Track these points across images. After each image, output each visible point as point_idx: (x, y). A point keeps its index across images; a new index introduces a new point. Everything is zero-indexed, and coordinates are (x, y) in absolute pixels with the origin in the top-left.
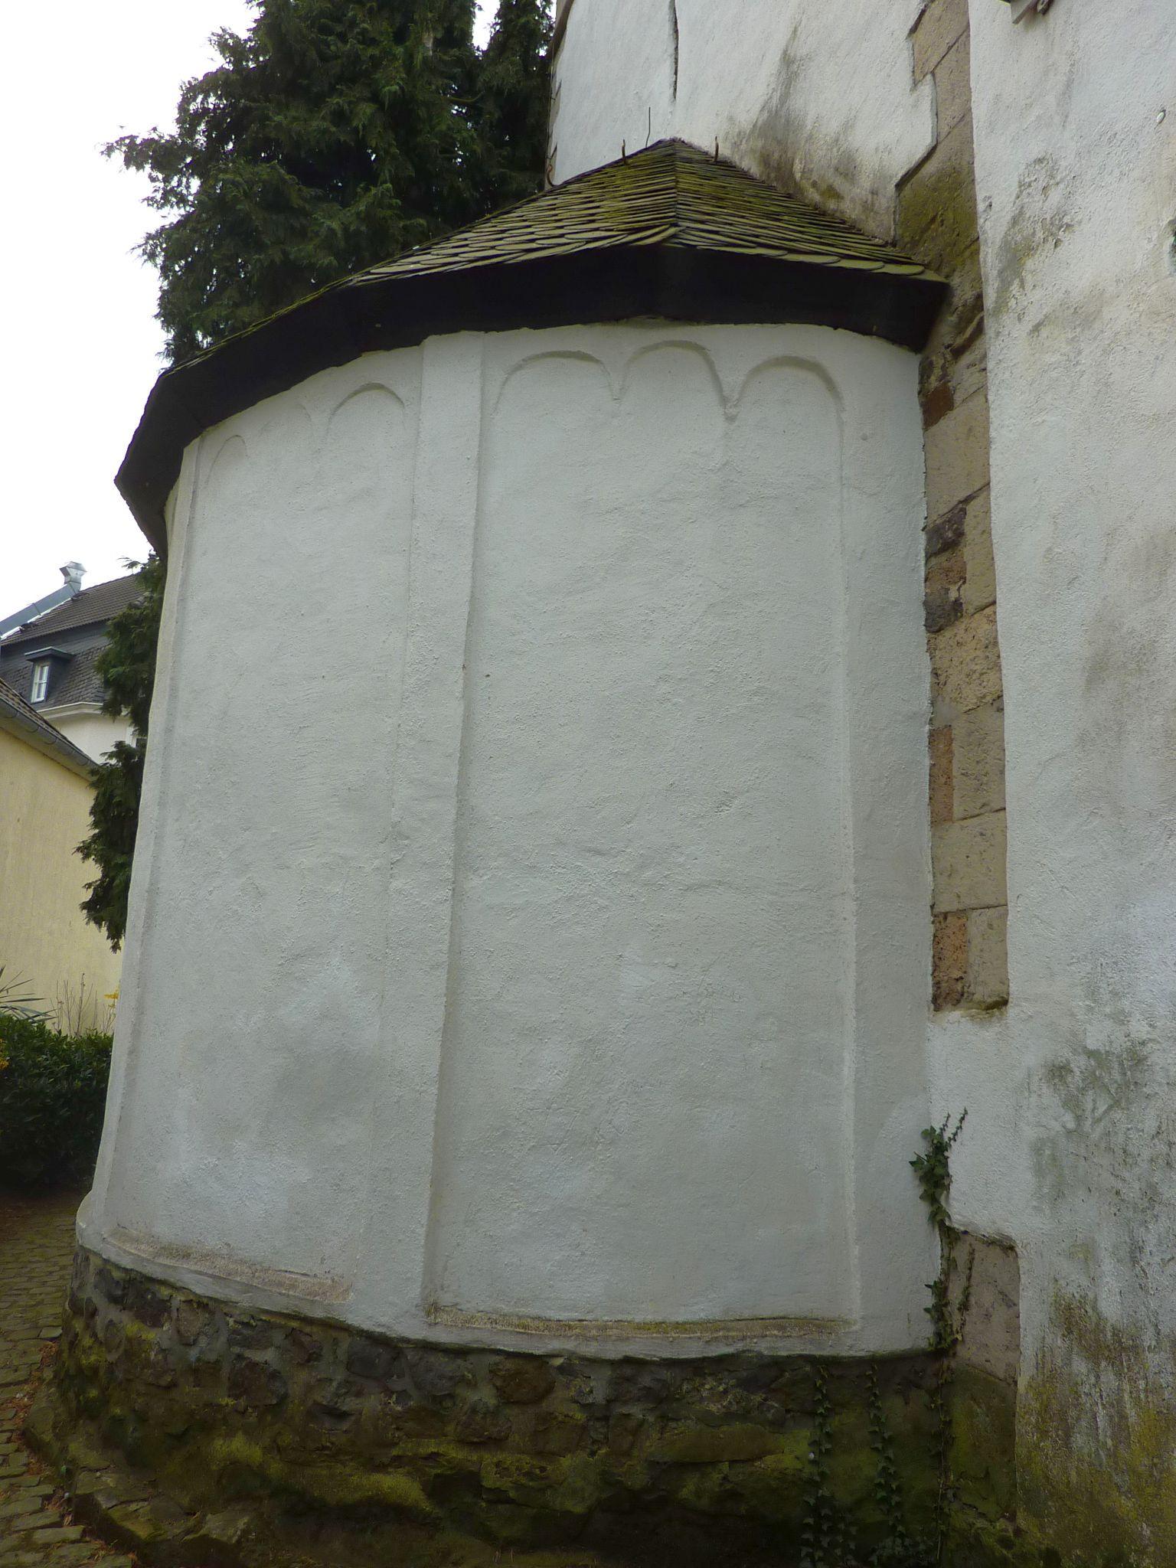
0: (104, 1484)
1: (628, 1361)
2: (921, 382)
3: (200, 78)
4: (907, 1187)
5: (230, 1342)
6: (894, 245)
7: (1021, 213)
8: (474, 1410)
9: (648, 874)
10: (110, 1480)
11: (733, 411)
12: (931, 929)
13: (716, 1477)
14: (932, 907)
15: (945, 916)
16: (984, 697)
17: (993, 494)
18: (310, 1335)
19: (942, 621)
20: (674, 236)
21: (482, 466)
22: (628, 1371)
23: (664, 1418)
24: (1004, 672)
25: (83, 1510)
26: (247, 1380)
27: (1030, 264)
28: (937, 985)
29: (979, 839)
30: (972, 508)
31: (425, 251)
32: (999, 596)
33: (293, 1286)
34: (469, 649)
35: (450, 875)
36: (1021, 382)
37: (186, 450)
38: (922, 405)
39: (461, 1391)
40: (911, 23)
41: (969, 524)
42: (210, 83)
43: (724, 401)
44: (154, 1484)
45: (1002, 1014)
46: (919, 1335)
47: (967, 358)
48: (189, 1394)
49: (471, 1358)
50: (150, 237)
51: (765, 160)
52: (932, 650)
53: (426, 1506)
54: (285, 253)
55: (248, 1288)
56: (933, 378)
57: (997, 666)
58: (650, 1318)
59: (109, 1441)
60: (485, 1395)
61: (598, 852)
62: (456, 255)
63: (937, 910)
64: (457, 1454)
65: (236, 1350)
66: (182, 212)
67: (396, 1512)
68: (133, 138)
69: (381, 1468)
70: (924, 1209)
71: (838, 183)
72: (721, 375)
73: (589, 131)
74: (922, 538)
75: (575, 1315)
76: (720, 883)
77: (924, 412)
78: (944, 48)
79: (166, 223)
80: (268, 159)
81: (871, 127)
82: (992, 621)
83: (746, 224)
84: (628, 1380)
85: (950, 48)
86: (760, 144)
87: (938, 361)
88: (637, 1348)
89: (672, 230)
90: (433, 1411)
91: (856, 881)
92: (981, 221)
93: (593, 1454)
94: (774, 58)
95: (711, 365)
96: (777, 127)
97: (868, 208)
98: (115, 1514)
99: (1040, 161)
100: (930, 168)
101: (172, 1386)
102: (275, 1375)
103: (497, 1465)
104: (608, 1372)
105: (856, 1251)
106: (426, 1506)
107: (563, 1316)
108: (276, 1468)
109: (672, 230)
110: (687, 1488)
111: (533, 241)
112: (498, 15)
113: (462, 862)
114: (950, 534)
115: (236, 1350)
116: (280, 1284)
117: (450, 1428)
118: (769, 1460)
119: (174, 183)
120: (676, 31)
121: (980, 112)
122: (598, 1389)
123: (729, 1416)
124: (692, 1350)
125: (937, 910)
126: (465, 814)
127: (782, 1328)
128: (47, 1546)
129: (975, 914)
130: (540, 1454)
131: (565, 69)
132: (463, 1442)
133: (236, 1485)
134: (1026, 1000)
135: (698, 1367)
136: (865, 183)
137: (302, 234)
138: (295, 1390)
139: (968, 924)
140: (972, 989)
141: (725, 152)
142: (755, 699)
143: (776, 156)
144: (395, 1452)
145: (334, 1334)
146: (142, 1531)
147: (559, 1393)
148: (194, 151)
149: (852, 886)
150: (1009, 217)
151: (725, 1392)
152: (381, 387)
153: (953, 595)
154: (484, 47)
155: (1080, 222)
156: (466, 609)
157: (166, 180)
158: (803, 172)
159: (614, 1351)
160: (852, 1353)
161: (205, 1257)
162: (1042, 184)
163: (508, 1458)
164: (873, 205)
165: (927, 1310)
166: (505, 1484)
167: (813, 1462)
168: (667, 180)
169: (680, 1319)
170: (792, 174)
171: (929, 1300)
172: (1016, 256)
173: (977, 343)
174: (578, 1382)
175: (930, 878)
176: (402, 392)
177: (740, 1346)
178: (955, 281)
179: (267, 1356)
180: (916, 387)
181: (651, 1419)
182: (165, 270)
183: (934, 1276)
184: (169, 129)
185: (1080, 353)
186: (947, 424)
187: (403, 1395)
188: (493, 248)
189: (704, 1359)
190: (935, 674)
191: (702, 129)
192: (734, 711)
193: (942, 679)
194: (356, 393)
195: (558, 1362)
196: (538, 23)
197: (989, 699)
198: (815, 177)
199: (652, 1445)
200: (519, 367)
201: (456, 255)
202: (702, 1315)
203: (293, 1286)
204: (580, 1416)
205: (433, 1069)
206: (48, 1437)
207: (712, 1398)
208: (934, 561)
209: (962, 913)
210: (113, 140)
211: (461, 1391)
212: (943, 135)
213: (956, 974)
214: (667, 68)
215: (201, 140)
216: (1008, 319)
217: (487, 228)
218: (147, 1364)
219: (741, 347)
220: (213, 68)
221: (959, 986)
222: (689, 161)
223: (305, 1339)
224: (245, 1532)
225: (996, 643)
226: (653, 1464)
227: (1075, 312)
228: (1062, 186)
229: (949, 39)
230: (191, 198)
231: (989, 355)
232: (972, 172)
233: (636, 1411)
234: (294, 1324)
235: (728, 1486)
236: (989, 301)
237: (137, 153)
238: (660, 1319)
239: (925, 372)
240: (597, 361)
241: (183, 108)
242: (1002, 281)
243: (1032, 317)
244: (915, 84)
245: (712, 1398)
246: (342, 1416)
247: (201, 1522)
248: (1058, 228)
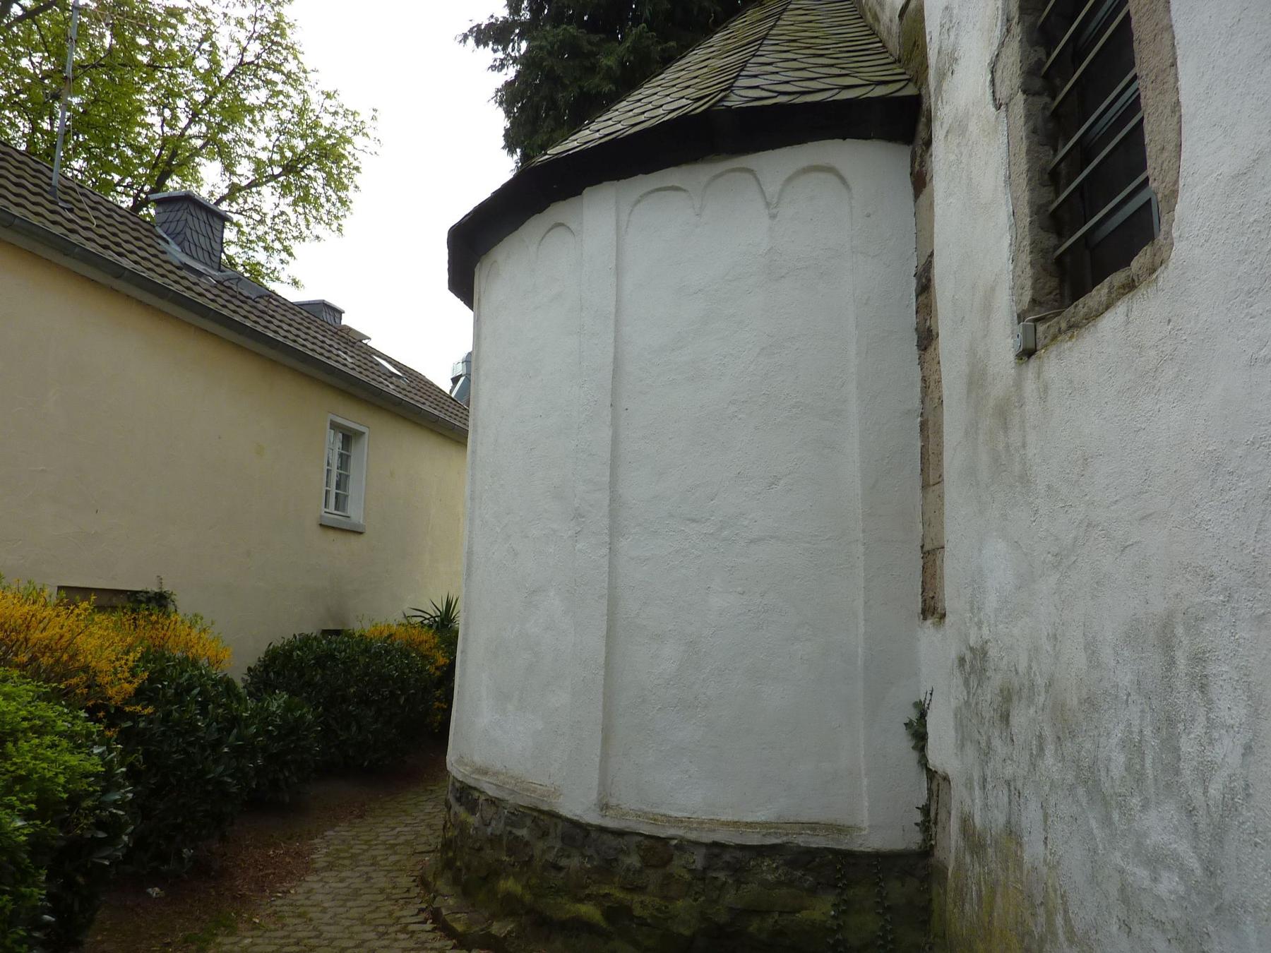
0: (448, 902)
1: (715, 844)
4: (904, 743)
5: (506, 824)
8: (628, 869)
10: (451, 902)
11: (774, 211)
13: (771, 921)
14: (922, 547)
18: (544, 820)
21: (619, 272)
22: (716, 851)
23: (739, 883)
25: (436, 916)
26: (515, 846)
28: (924, 601)
33: (534, 792)
34: (615, 393)
35: (607, 539)
37: (476, 270)
39: (621, 857)
43: (768, 205)
44: (473, 905)
46: (914, 840)
48: (488, 854)
49: (626, 838)
50: (498, 91)
53: (603, 924)
54: (581, 88)
55: (512, 792)
58: (730, 818)
59: (456, 881)
60: (634, 861)
61: (694, 521)
64: (619, 894)
65: (509, 828)
67: (581, 926)
68: (479, 26)
69: (581, 901)
70: (914, 755)
74: (914, 282)
75: (686, 815)
76: (772, 537)
84: (716, 856)
87: (919, 152)
88: (721, 836)
90: (607, 868)
91: (864, 531)
93: (696, 900)
98: (448, 918)
101: (480, 849)
102: (527, 844)
103: (642, 902)
104: (704, 850)
105: (865, 781)
106: (603, 924)
107: (679, 815)
108: (528, 898)
110: (754, 926)
113: (615, 532)
115: (509, 828)
116: (528, 790)
117: (616, 879)
118: (805, 914)
119: (510, 50)
122: (698, 860)
123: (779, 883)
124: (754, 839)
125: (926, 549)
126: (615, 500)
127: (814, 829)
128: (413, 932)
130: (665, 898)
132: (623, 888)
133: (510, 906)
135: (760, 851)
137: (592, 70)
138: (537, 852)
144: (587, 892)
145: (555, 820)
146: (459, 927)
147: (676, 862)
148: (522, 24)
151: (777, 868)
157: (504, 49)
159: (707, 838)
160: (862, 849)
161: (496, 774)
163: (647, 899)
165: (917, 824)
166: (646, 914)
167: (833, 917)
169: (749, 820)
171: (919, 817)
172: (942, 76)
174: (686, 856)
176: (573, 227)
177: (785, 839)
179: (523, 832)
181: (730, 881)
183: (922, 802)
184: (502, 13)
187: (591, 858)
189: (762, 846)
190: (924, 380)
195: (675, 842)
199: (730, 898)
200: (639, 201)
202: (763, 818)
203: (534, 792)
204: (687, 876)
205: (602, 660)
206: (430, 879)
207: (768, 871)
210: (466, 31)
211: (621, 857)
218: (470, 836)
219: (775, 165)
223: (541, 823)
224: (510, 932)
226: (731, 909)
233: (722, 876)
234: (535, 814)
238: (736, 819)
245: (768, 871)
246: (560, 869)
247: (491, 925)
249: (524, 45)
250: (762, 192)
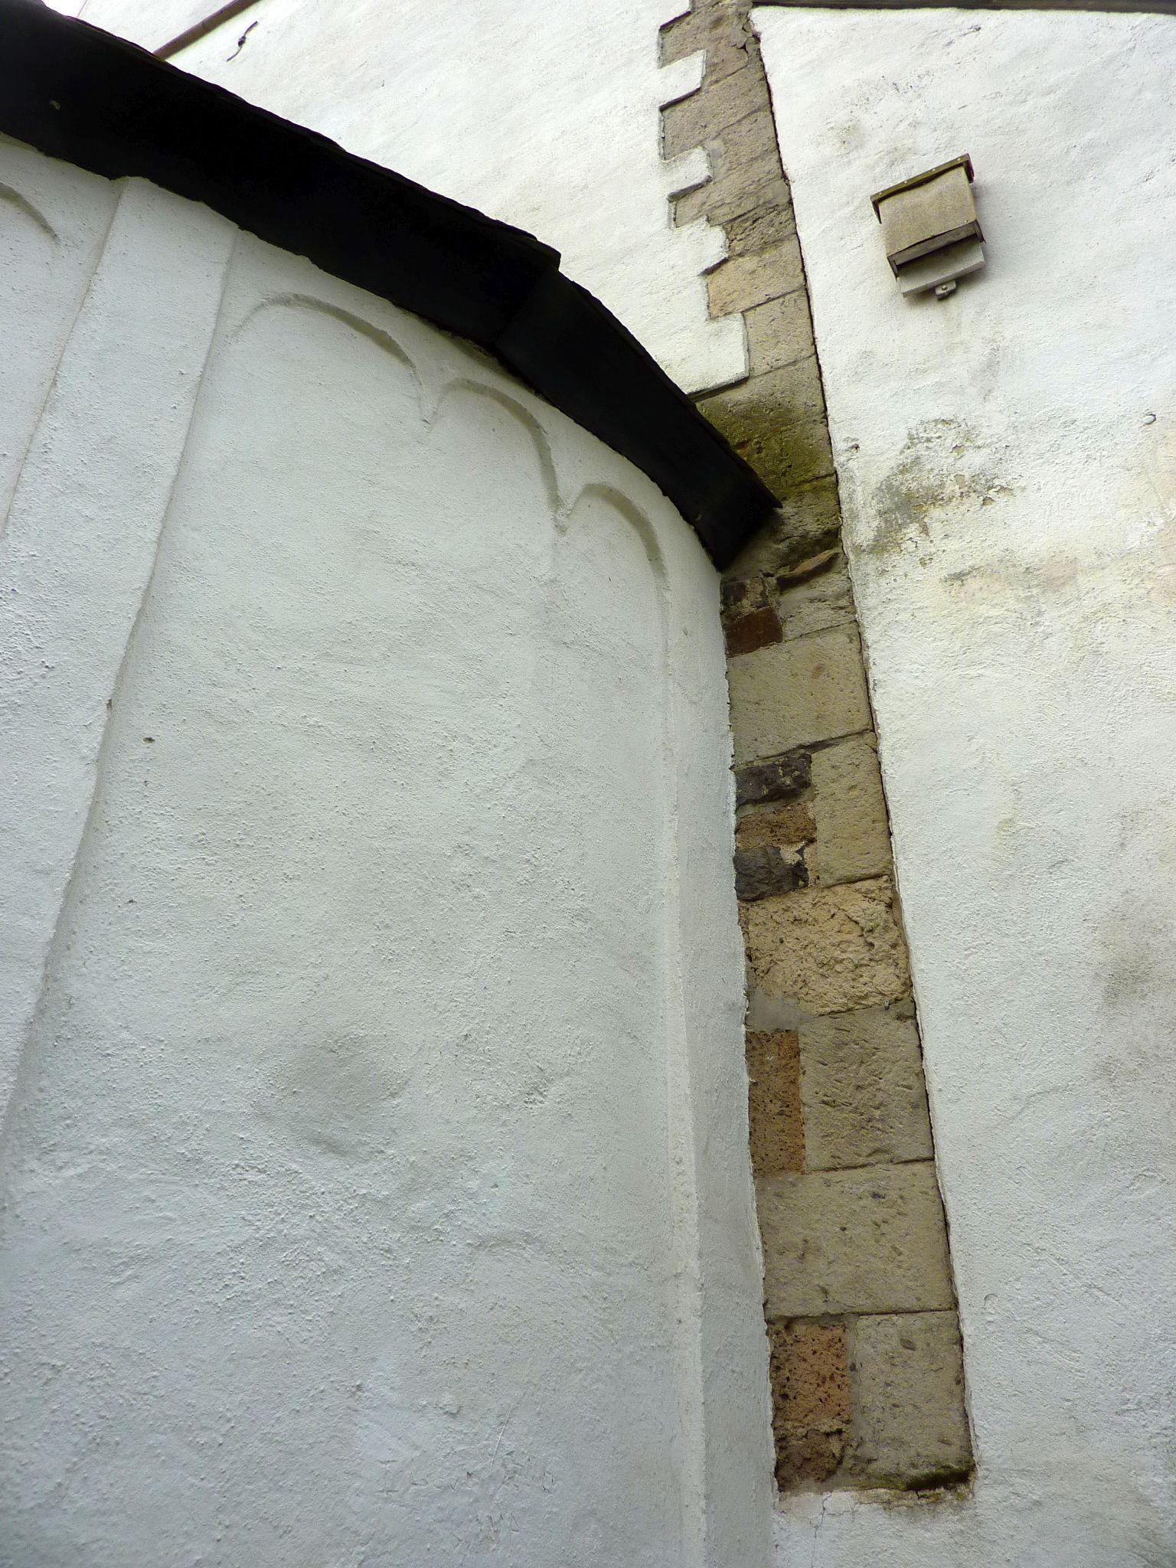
9: (419, 1206)
12: (765, 1347)
15: (790, 1322)
19: (764, 888)
28: (781, 1442)
29: (869, 1202)
38: (724, 627)
43: (556, 501)
45: (962, 1498)
52: (744, 923)
63: (774, 1313)
74: (731, 778)
76: (529, 1239)
77: (728, 636)
100: (740, 395)
129: (864, 1321)
134: (1022, 1472)
139: (849, 1338)
140: (868, 1450)
142: (578, 924)
149: (694, 1264)
153: (789, 855)
155: (1024, 489)
156: (134, 602)
173: (821, 580)
175: (759, 1258)
180: (719, 607)
192: (549, 934)
193: (763, 964)
208: (750, 810)
209: (837, 1320)
212: (761, 367)
213: (827, 1424)
221: (835, 1446)
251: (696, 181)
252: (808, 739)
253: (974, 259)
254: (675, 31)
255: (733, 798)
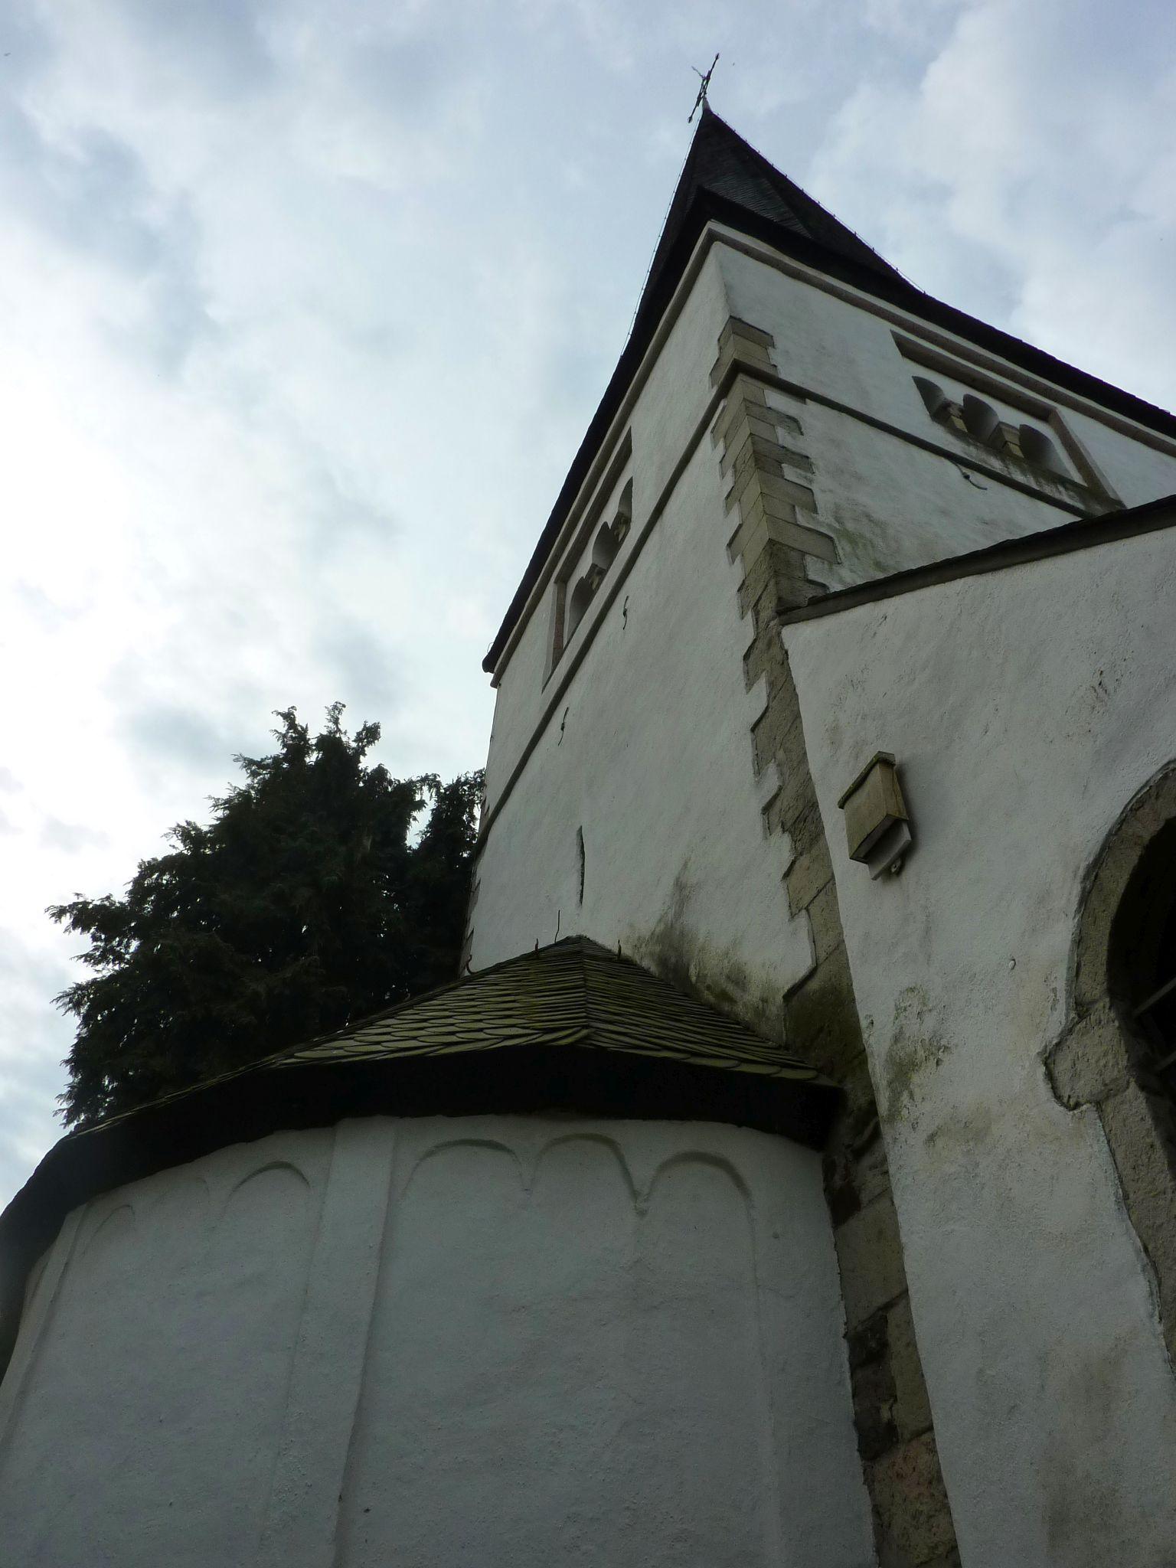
2: (825, 1179)
3: (160, 859)
6: (787, 1048)
7: (901, 1032)
16: (936, 1547)
17: (913, 1305)
20: (587, 1037)
24: (955, 1516)
27: (916, 1079)
30: (894, 1316)
31: (349, 1033)
32: (935, 1422)
36: (917, 1172)
40: (785, 869)
41: (892, 1332)
42: (168, 864)
43: (635, 1194)
47: (867, 1161)
51: (663, 962)
52: (870, 1481)
56: (837, 1177)
57: (945, 1508)
62: (378, 1043)
66: (117, 968)
68: (85, 904)
71: (730, 988)
72: (631, 1170)
73: (503, 927)
78: (814, 892)
79: (99, 976)
80: (208, 928)
81: (759, 948)
82: (933, 1451)
83: (650, 1025)
85: (819, 892)
86: (658, 949)
89: (585, 1032)
92: (865, 1036)
94: (668, 883)
95: (621, 1160)
96: (673, 944)
97: (760, 1013)
99: (912, 990)
100: (814, 985)
109: (585, 1032)
111: (453, 1033)
112: (429, 826)
114: (873, 1345)
119: (115, 943)
120: (583, 853)
121: (852, 945)
131: (484, 869)
136: (753, 995)
141: (627, 951)
143: (673, 960)
148: (139, 917)
150: (890, 1035)
152: (287, 1166)
153: (885, 1415)
154: (415, 847)
157: (108, 940)
158: (698, 976)
162: (916, 1009)
164: (764, 1010)
168: (576, 977)
170: (688, 977)
172: (903, 1071)
178: (848, 1086)
180: (822, 1185)
182: (87, 1020)
185: (977, 1164)
186: (857, 1225)
188: (414, 1038)
190: (877, 1511)
191: (608, 931)
194: (261, 1171)
196: (463, 833)
197: (941, 1550)
198: (709, 981)
201: (378, 1043)
212: (823, 955)
214: (575, 879)
215: (148, 908)
216: (902, 1128)
217: (409, 1014)
219: (649, 1143)
220: (174, 852)
222: (594, 958)
225: (940, 1479)
227: (966, 1126)
228: (934, 1013)
229: (819, 883)
230: (127, 956)
231: (890, 1159)
232: (851, 992)
235: (107, 903)
236: (883, 1106)
237: (84, 916)
239: (829, 1170)
240: (509, 1151)
241: (138, 882)
242: (893, 1091)
243: (926, 1128)
244: (793, 916)
248: (937, 1049)
249: (135, 944)
250: (626, 1174)
251: (773, 793)
252: (881, 1300)
253: (906, 835)
254: (752, 657)
255: (847, 1365)
